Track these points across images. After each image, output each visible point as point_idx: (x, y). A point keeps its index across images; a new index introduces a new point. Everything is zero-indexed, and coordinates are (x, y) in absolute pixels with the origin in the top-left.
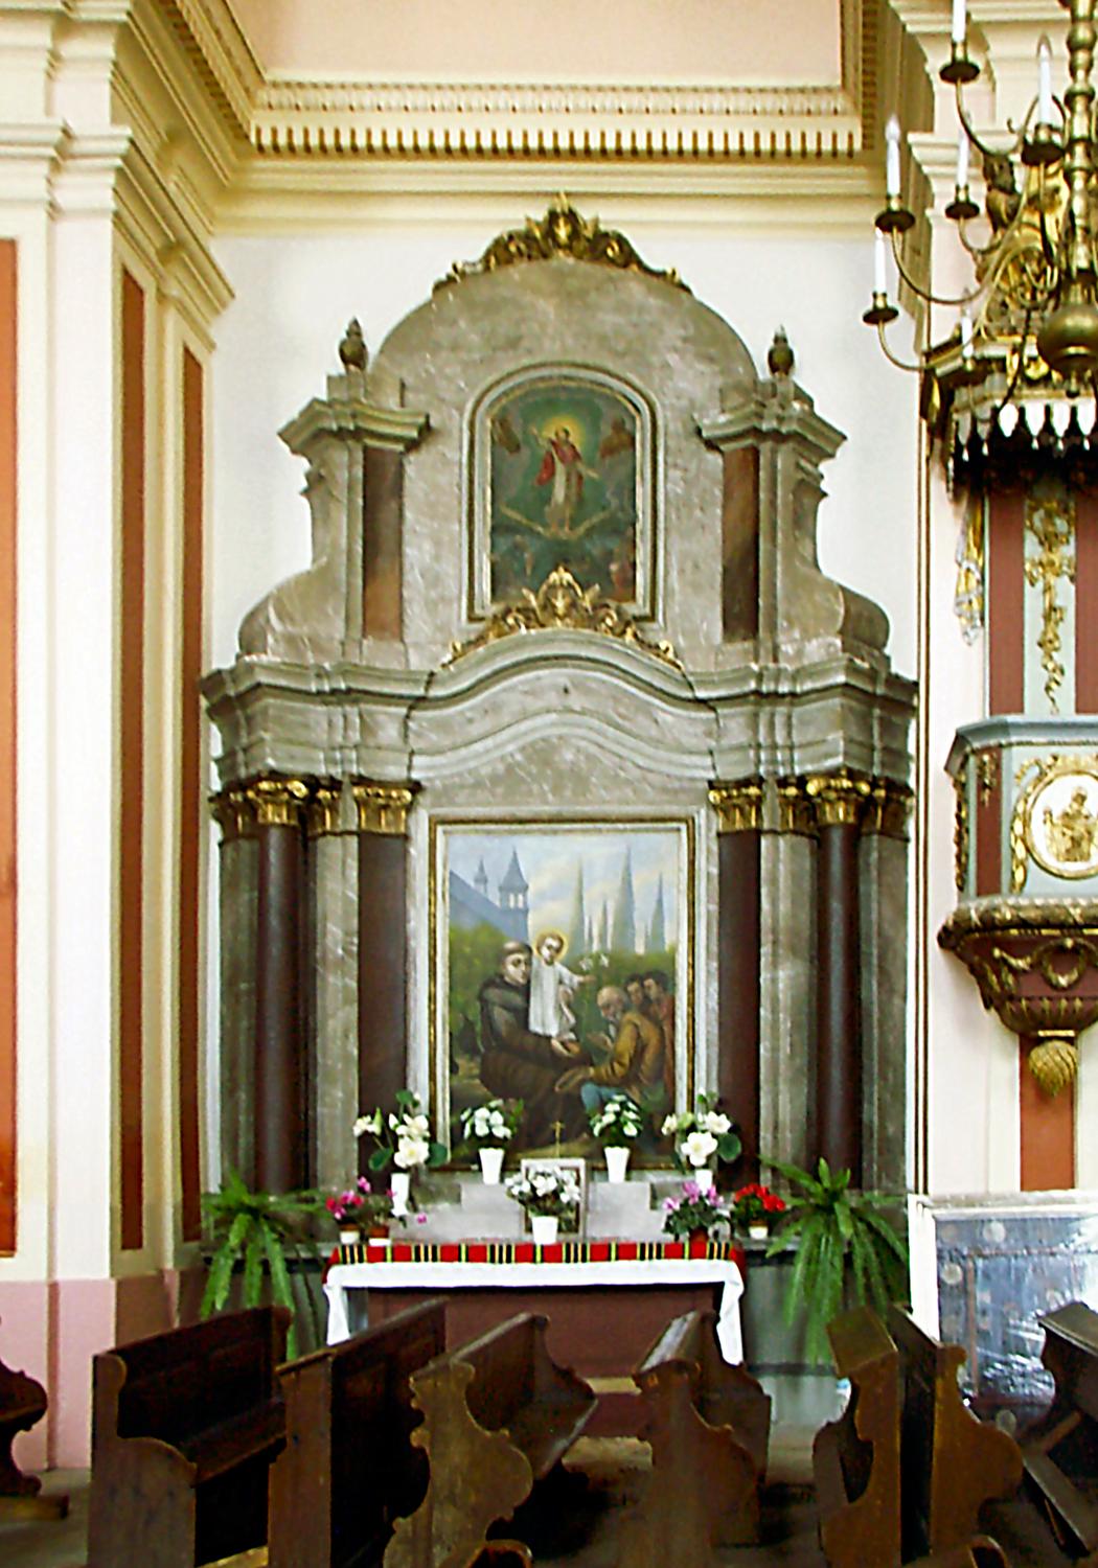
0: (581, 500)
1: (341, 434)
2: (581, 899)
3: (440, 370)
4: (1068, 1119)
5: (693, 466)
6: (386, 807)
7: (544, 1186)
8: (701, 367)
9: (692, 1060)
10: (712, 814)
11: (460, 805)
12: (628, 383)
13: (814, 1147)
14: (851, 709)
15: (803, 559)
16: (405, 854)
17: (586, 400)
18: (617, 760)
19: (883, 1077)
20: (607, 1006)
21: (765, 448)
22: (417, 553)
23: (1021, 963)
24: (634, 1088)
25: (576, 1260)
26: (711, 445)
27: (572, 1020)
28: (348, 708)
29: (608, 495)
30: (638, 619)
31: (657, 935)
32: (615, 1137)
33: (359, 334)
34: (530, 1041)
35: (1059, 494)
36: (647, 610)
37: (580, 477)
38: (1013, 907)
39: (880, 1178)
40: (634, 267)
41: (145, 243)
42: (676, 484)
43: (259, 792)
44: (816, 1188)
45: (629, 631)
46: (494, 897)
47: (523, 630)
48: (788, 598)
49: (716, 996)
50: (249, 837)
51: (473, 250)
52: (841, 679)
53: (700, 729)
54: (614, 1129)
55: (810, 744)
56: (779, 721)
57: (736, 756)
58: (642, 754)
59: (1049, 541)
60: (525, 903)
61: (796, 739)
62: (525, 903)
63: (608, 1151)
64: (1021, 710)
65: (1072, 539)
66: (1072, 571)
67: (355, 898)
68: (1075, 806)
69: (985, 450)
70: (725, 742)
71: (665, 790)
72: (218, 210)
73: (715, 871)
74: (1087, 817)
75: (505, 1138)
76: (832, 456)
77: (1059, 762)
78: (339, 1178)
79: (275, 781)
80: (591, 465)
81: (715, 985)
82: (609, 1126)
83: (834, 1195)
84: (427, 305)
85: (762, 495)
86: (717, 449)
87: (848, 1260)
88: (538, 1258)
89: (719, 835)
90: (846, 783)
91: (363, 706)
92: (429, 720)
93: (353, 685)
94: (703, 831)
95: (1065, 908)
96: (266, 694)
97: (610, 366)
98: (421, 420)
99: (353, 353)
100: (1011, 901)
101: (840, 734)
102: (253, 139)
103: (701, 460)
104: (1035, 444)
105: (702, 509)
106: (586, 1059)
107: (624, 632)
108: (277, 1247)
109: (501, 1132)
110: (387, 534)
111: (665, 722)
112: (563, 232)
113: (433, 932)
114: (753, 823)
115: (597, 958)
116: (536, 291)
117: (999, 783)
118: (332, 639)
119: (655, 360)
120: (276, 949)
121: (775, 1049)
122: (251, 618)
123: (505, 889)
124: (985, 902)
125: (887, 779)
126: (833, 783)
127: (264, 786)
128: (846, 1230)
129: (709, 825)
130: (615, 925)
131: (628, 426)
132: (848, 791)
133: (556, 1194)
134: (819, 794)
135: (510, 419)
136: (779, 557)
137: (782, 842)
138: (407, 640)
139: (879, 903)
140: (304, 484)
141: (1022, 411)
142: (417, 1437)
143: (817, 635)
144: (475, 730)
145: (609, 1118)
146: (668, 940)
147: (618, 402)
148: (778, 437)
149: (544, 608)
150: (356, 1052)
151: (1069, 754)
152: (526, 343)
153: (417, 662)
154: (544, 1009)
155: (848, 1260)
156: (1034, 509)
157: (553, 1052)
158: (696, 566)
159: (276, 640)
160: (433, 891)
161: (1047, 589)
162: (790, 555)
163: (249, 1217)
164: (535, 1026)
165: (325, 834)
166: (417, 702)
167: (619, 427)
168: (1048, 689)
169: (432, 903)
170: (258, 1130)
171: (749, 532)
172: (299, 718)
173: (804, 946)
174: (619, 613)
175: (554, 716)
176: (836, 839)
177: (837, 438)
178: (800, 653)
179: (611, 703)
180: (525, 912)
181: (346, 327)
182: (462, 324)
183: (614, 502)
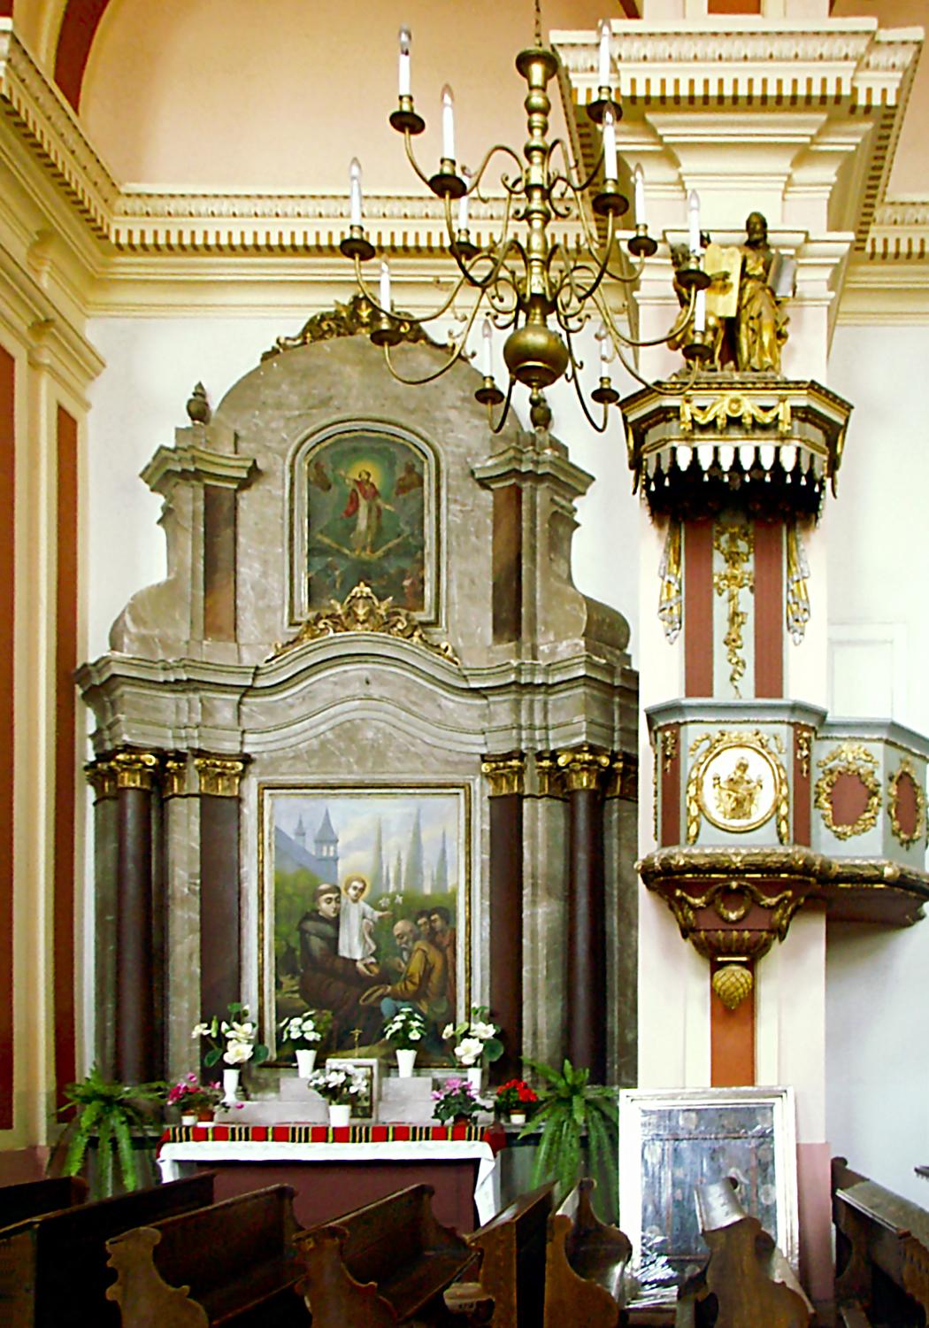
0: (380, 529)
1: (184, 474)
2: (380, 849)
3: (267, 423)
4: (749, 1029)
5: (470, 501)
6: (221, 775)
7: (336, 1080)
8: (476, 422)
9: (469, 980)
10: (485, 781)
11: (283, 774)
12: (418, 435)
13: (566, 1048)
14: (593, 697)
15: (559, 577)
16: (239, 813)
17: (383, 447)
18: (409, 738)
19: (623, 994)
20: (401, 936)
21: (526, 485)
22: (248, 571)
23: (698, 902)
24: (424, 1003)
25: (360, 1141)
26: (484, 483)
27: (374, 947)
28: (191, 695)
29: (402, 525)
30: (424, 624)
31: (441, 878)
32: (402, 1040)
33: (203, 396)
34: (339, 965)
35: (742, 521)
36: (432, 618)
37: (379, 510)
38: (686, 855)
39: (620, 1075)
40: (422, 342)
41: (17, 321)
42: (455, 515)
43: (118, 762)
44: (561, 1083)
45: (416, 634)
46: (311, 848)
47: (331, 634)
48: (546, 609)
49: (488, 930)
50: (115, 798)
51: (293, 327)
52: (582, 672)
53: (475, 713)
54: (401, 1034)
55: (558, 726)
56: (538, 707)
57: (501, 735)
58: (428, 733)
59: (732, 558)
60: (335, 851)
61: (551, 722)
62: (335, 851)
63: (399, 1052)
64: (711, 695)
65: (751, 557)
66: (751, 584)
67: (198, 848)
68: (739, 773)
69: (667, 483)
70: (495, 724)
71: (447, 762)
72: (92, 297)
73: (487, 827)
74: (748, 782)
75: (315, 1041)
76: (583, 494)
77: (725, 738)
78: (185, 1075)
79: (131, 754)
80: (387, 501)
81: (487, 921)
82: (398, 1031)
83: (575, 1090)
84: (258, 369)
85: (524, 524)
86: (488, 488)
87: (584, 1142)
88: (331, 1138)
89: (490, 798)
90: (587, 757)
91: (202, 693)
92: (257, 705)
93: (192, 677)
94: (478, 796)
95: (728, 856)
96: (123, 683)
97: (403, 421)
98: (249, 464)
99: (198, 409)
100: (685, 851)
101: (582, 717)
102: (113, 239)
103: (475, 497)
104: (706, 478)
105: (477, 537)
106: (386, 977)
107: (412, 635)
108: (124, 1127)
109: (310, 1036)
110: (224, 556)
111: (447, 707)
112: (365, 313)
113: (261, 875)
114: (516, 789)
115: (393, 899)
116: (345, 361)
117: (678, 754)
118: (179, 640)
119: (438, 414)
120: (132, 887)
121: (534, 971)
122: (116, 623)
123: (320, 842)
124: (666, 851)
125: (625, 754)
126: (578, 756)
127: (121, 757)
128: (579, 1117)
129: (482, 790)
130: (407, 870)
131: (417, 469)
132: (590, 763)
133: (347, 1084)
134: (567, 766)
135: (322, 463)
136: (538, 574)
137: (541, 804)
138: (241, 641)
139: (619, 855)
140: (160, 514)
141: (695, 451)
142: (112, 1292)
143: (566, 638)
144: (295, 713)
145: (398, 1026)
146: (450, 884)
147: (410, 450)
148: (541, 478)
149: (348, 615)
150: (198, 971)
151: (734, 731)
152: (335, 403)
153: (249, 659)
154: (351, 938)
155: (584, 1142)
156: (722, 533)
157: (357, 972)
158: (473, 582)
159: (131, 640)
160: (261, 843)
161: (732, 598)
162: (548, 572)
163: (102, 1104)
164: (344, 952)
165: (174, 796)
166: (247, 691)
167: (410, 469)
168: (732, 679)
169: (261, 852)
170: (118, 1033)
171: (513, 557)
172: (151, 703)
173: (559, 889)
174: (407, 620)
175: (358, 702)
176: (582, 802)
177: (586, 479)
178: (553, 652)
179: (403, 692)
180: (336, 860)
181: (193, 390)
182: (285, 387)
183: (407, 530)
